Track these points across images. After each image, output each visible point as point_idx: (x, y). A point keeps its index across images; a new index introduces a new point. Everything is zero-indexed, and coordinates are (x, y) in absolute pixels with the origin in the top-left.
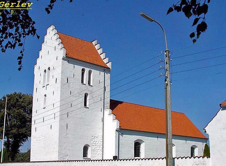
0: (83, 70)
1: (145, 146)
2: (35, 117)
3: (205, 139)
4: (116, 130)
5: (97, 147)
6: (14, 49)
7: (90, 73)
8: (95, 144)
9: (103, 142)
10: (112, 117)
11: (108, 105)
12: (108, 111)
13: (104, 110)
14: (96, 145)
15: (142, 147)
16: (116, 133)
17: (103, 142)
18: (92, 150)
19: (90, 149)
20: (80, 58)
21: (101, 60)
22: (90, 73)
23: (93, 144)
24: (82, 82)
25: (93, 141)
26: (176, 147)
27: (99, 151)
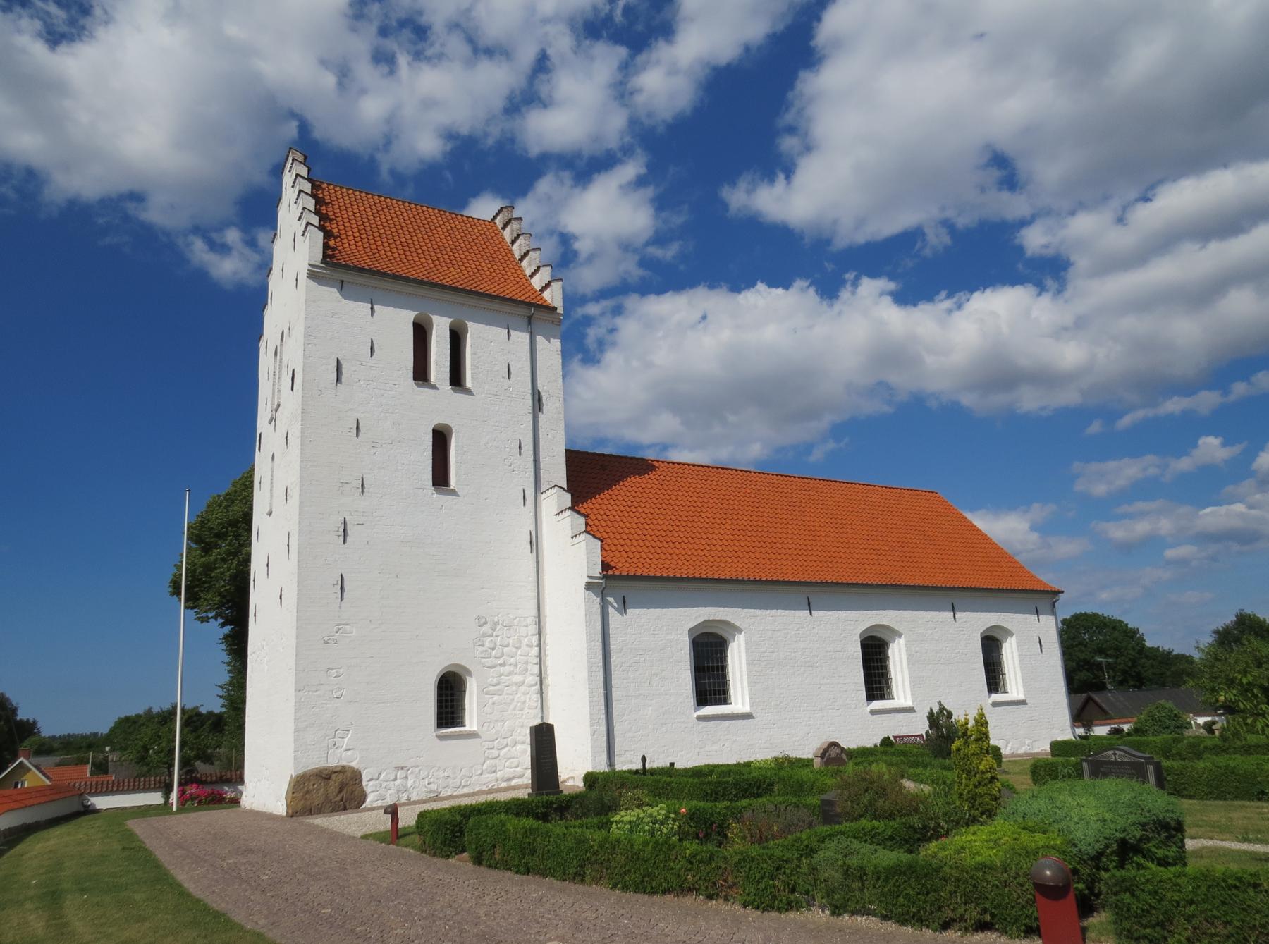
0: (421, 334)
1: (747, 649)
2: (247, 700)
3: (1047, 592)
4: (589, 586)
5: (510, 674)
6: (195, 619)
7: (457, 340)
8: (501, 661)
9: (539, 646)
10: (572, 522)
11: (556, 470)
12: (555, 500)
13: (536, 497)
14: (503, 665)
15: (897, 656)
16: (587, 601)
17: (539, 646)
18: (482, 691)
19: (475, 684)
20: (413, 274)
21: (524, 281)
22: (457, 340)
23: (489, 662)
24: (421, 373)
25: (487, 645)
26: (1017, 636)
27: (523, 689)
